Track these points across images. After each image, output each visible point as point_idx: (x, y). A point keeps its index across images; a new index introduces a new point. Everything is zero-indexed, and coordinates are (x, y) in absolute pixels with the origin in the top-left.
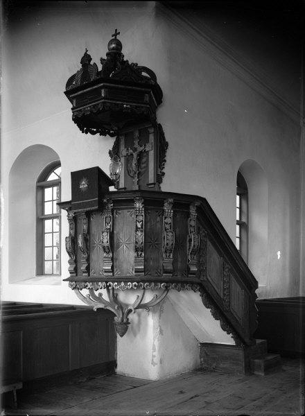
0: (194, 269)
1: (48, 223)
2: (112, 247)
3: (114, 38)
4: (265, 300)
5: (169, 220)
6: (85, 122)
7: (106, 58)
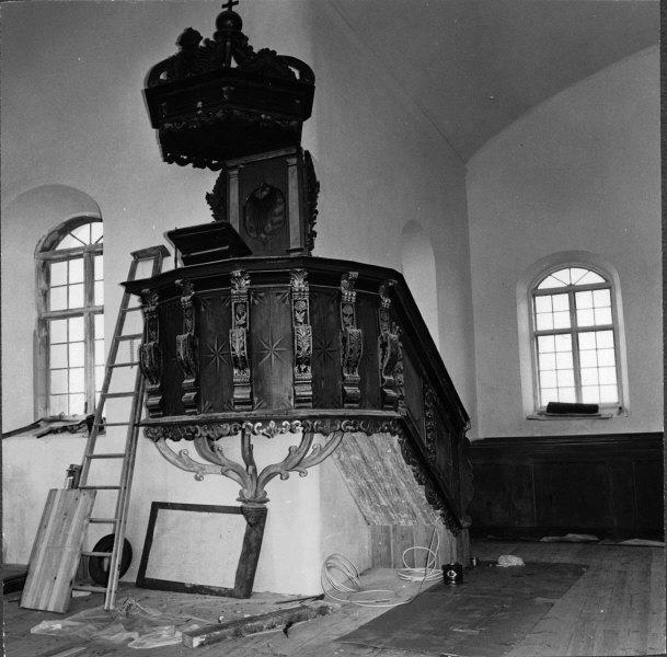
1: (57, 327)
3: (226, 9)
4: (486, 440)
6: (177, 148)
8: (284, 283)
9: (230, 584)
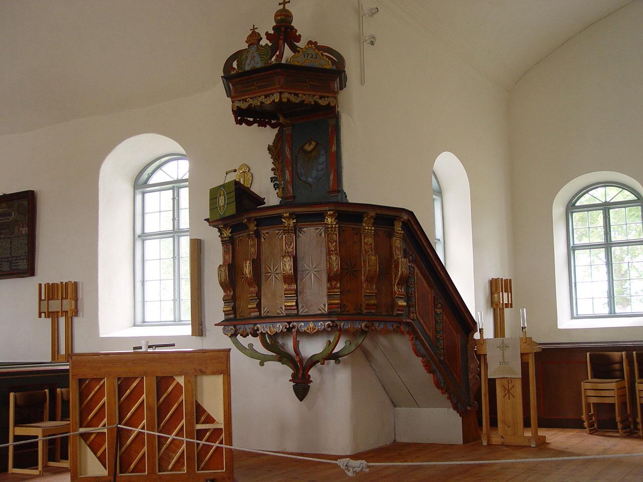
0: (402, 303)
2: (293, 279)
5: (370, 240)
7: (272, 32)
8: (322, 221)
9: (50, 360)
